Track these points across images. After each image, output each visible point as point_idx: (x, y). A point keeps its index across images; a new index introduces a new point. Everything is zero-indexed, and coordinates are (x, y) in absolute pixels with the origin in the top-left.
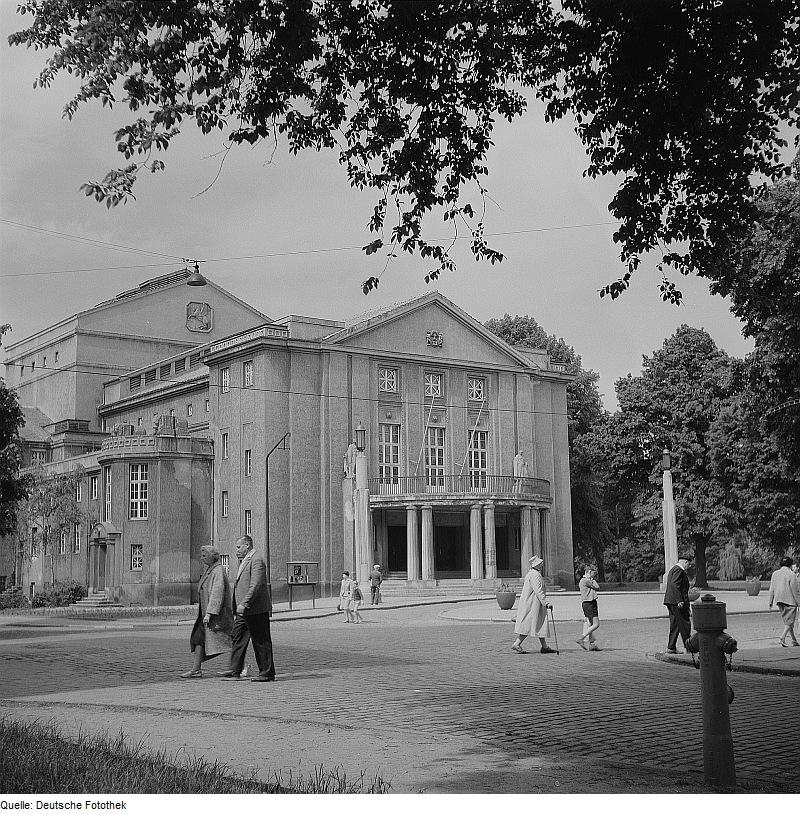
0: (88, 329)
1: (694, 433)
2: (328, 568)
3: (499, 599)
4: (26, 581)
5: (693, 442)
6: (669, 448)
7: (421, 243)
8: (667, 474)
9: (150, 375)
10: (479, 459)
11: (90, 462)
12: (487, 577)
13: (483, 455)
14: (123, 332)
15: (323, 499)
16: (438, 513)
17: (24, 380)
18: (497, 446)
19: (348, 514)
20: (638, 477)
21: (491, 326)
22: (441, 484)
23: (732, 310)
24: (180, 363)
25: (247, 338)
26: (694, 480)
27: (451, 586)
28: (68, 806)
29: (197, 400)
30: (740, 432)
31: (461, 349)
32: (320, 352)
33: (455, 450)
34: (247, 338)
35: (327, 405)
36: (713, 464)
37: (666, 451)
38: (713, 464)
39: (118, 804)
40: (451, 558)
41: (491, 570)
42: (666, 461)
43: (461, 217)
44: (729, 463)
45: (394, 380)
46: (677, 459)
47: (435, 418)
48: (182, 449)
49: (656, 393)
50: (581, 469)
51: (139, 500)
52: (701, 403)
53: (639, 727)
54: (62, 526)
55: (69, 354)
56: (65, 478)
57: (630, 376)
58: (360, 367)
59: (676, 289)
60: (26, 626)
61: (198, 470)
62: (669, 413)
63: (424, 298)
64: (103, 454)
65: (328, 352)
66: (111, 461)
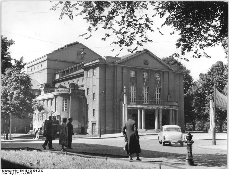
29: (80, 79)
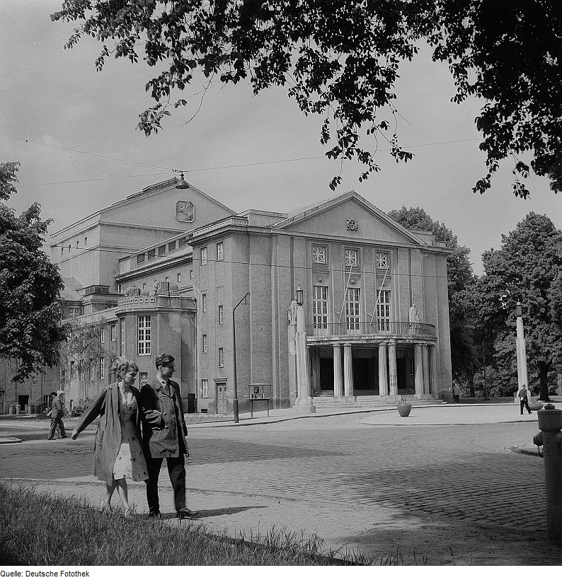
0: (108, 220)
9: (151, 253)
10: (384, 311)
11: (110, 315)
16: (355, 349)
25: (219, 226)
28: (48, 574)
29: (184, 270)
32: (271, 236)
34: (219, 226)
39: (84, 573)
41: (394, 389)
48: (174, 305)
61: (186, 320)
65: (276, 235)
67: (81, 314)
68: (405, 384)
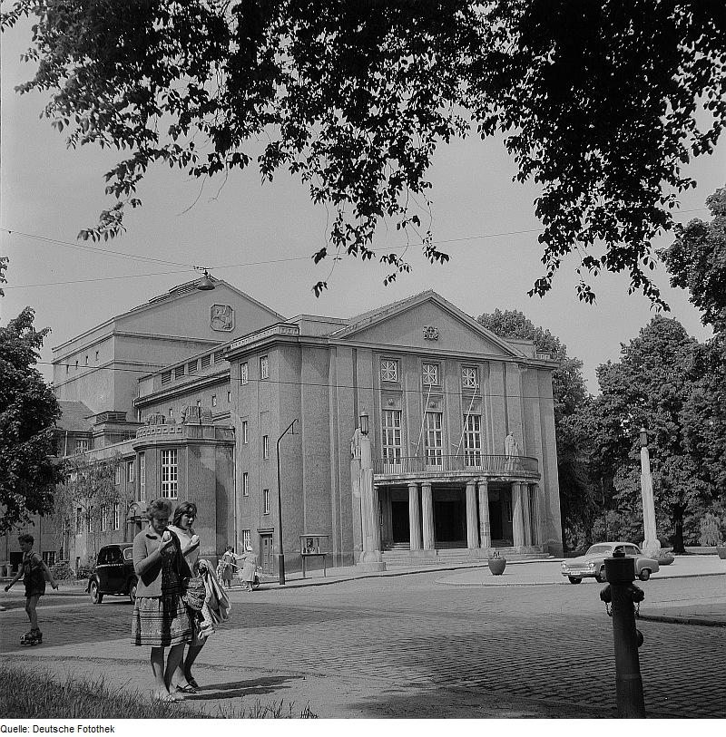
1: (669, 413)
2: (339, 540)
3: (491, 565)
4: (73, 555)
5: (668, 421)
6: (646, 427)
7: (362, 248)
8: (644, 452)
10: (473, 441)
11: (126, 448)
12: (482, 546)
13: (477, 436)
14: (154, 333)
15: (333, 479)
16: (437, 490)
17: (70, 377)
18: (490, 428)
19: (356, 492)
20: (620, 451)
21: (483, 320)
22: (439, 463)
23: (692, 301)
24: (206, 359)
25: (263, 335)
26: (670, 455)
27: (450, 555)
28: (61, 730)
29: (220, 391)
30: (710, 411)
31: (456, 342)
32: (328, 347)
33: (451, 433)
34: (263, 335)
35: (335, 394)
36: (686, 440)
37: (643, 430)
38: (686, 440)
39: (107, 728)
40: (449, 529)
41: (486, 539)
42: (643, 439)
43: (411, 226)
44: (701, 439)
45: (395, 371)
46: (653, 436)
47: (432, 403)
48: (207, 435)
49: (633, 377)
50: (567, 447)
51: (169, 482)
52: (675, 385)
53: (582, 672)
54: (103, 506)
55: (108, 353)
56: (105, 463)
57: (609, 363)
58: (365, 364)
59: (591, 291)
60: (63, 595)
61: (221, 454)
62: (645, 395)
63: (420, 295)
64: (137, 441)
65: (335, 346)
66: (145, 447)
67: (90, 448)
68: (500, 533)
